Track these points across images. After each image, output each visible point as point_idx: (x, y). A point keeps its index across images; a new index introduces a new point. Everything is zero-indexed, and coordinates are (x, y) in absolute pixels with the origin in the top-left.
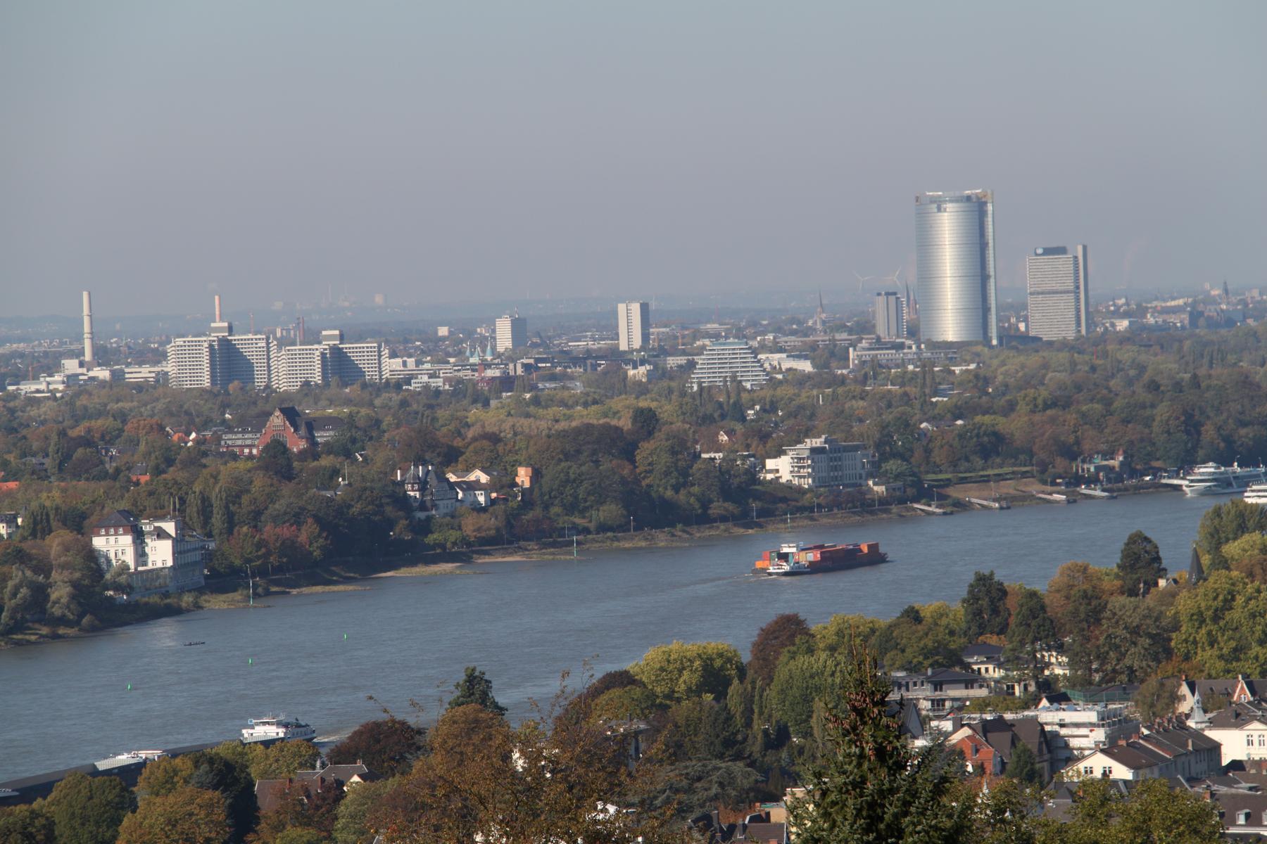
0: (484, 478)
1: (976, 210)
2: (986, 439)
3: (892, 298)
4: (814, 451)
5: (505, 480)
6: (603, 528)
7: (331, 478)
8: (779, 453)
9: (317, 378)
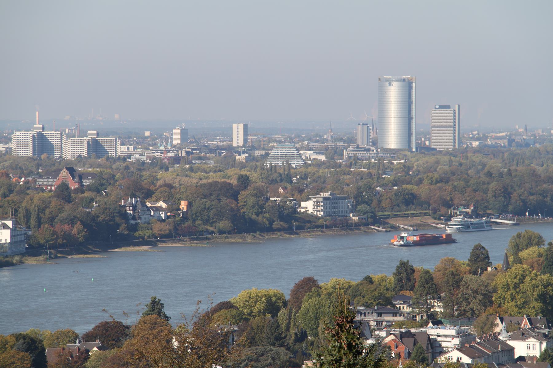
0: (164, 205)
1: (408, 86)
2: (407, 196)
3: (365, 127)
4: (324, 198)
5: (175, 207)
6: (221, 232)
7: (90, 202)
8: (308, 199)
9: (85, 154)
